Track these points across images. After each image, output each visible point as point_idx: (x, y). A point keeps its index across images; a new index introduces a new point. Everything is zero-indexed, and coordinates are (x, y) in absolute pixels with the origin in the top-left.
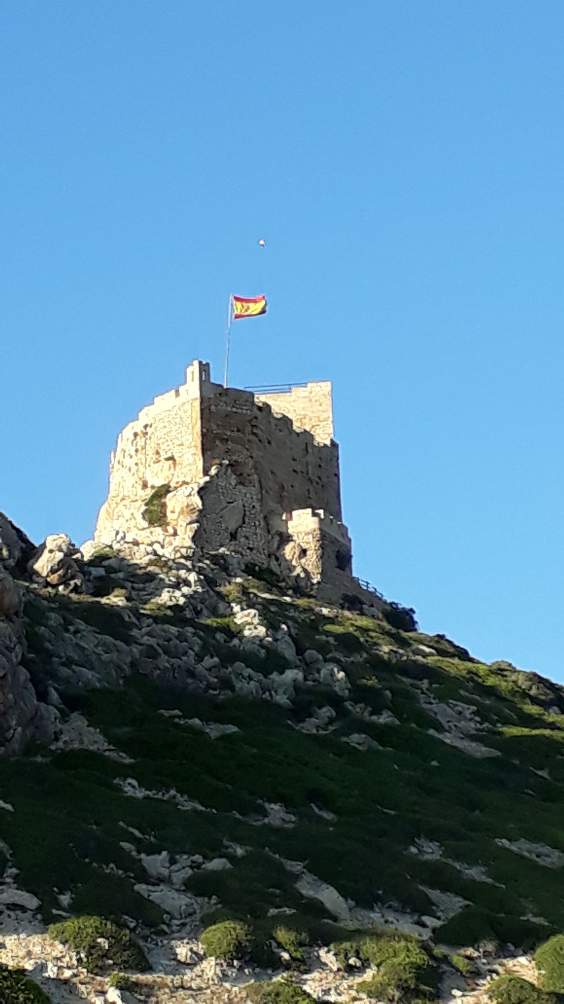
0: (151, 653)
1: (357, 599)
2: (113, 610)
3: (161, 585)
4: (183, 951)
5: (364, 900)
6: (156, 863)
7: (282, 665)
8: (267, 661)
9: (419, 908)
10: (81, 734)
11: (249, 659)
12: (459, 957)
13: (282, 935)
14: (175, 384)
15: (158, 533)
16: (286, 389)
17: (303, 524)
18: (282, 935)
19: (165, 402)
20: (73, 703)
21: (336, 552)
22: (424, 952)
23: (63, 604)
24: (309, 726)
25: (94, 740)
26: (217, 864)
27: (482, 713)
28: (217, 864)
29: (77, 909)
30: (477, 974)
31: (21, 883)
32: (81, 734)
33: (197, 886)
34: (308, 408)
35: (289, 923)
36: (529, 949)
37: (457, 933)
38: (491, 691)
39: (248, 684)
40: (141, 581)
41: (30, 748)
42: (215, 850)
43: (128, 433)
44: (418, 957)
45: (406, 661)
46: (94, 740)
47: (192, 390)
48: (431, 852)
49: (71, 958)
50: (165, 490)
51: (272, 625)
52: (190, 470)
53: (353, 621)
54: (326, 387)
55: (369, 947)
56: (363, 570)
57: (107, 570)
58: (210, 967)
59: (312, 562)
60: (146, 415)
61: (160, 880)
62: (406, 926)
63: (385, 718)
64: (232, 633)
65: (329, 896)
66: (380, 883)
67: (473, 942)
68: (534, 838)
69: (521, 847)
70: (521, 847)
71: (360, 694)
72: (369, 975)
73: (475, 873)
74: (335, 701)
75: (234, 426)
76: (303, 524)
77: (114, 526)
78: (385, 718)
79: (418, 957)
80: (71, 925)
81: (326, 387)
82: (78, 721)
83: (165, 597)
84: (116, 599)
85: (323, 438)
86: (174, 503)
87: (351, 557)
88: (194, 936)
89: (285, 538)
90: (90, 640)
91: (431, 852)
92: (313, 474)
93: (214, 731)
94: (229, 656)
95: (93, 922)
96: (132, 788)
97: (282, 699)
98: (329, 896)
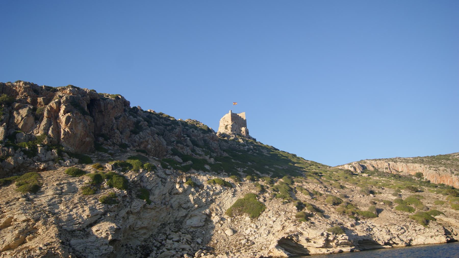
0: (231, 145)
1: (250, 138)
2: (225, 140)
3: (230, 137)
4: (245, 179)
5: (262, 173)
6: (239, 169)
7: (245, 146)
8: (244, 145)
9: (268, 174)
10: (225, 154)
11: (242, 145)
12: (275, 179)
13: (255, 177)
14: (228, 113)
15: (227, 130)
16: (240, 113)
17: (243, 129)
18: (255, 177)
19: (227, 115)
20: (224, 151)
21: (247, 132)
22: (76, 160)
23: (220, 139)
24: (249, 153)
25: (227, 155)
26: (245, 169)
27: (268, 151)
28: (245, 169)
29: (232, 175)
30: (277, 181)
31: (225, 172)
32: (225, 154)
33: (244, 172)
34: (242, 115)
35: (256, 176)
36: (282, 178)
37: (273, 177)
38: (267, 148)
39: (242, 148)
40: (229, 136)
41: (220, 156)
42: (245, 168)
43: (222, 118)
44: (270, 179)
45: (14, 90)
46: (227, 155)
47: (230, 113)
48: (267, 167)
49: (233, 180)
50: (227, 125)
51: (244, 141)
52: (230, 123)
53: (251, 140)
54: (244, 113)
55: (265, 178)
56: (250, 134)
57: (224, 135)
58: (248, 181)
59: (244, 133)
60: (224, 117)
61: (239, 171)
62: (267, 176)
63: (257, 152)
64: (239, 142)
65: (258, 173)
66: (265, 172)
67: (275, 177)
68: (278, 165)
69: (276, 166)
70: (276, 166)
71: (254, 149)
72: (265, 181)
73: (273, 169)
74: (252, 150)
75: (235, 117)
76: (243, 129)
77: (221, 130)
78: (257, 152)
79: (270, 179)
80: (232, 176)
81: (244, 113)
82: (225, 153)
83: (231, 138)
84: (226, 138)
85: (244, 119)
86: (228, 127)
87: (93, 93)
88: (245, 177)
89: (241, 131)
90: (224, 143)
91: (267, 167)
92: (244, 123)
93: (240, 154)
94: (240, 145)
95: (234, 176)
96: (233, 161)
97: (246, 150)
98: (258, 173)
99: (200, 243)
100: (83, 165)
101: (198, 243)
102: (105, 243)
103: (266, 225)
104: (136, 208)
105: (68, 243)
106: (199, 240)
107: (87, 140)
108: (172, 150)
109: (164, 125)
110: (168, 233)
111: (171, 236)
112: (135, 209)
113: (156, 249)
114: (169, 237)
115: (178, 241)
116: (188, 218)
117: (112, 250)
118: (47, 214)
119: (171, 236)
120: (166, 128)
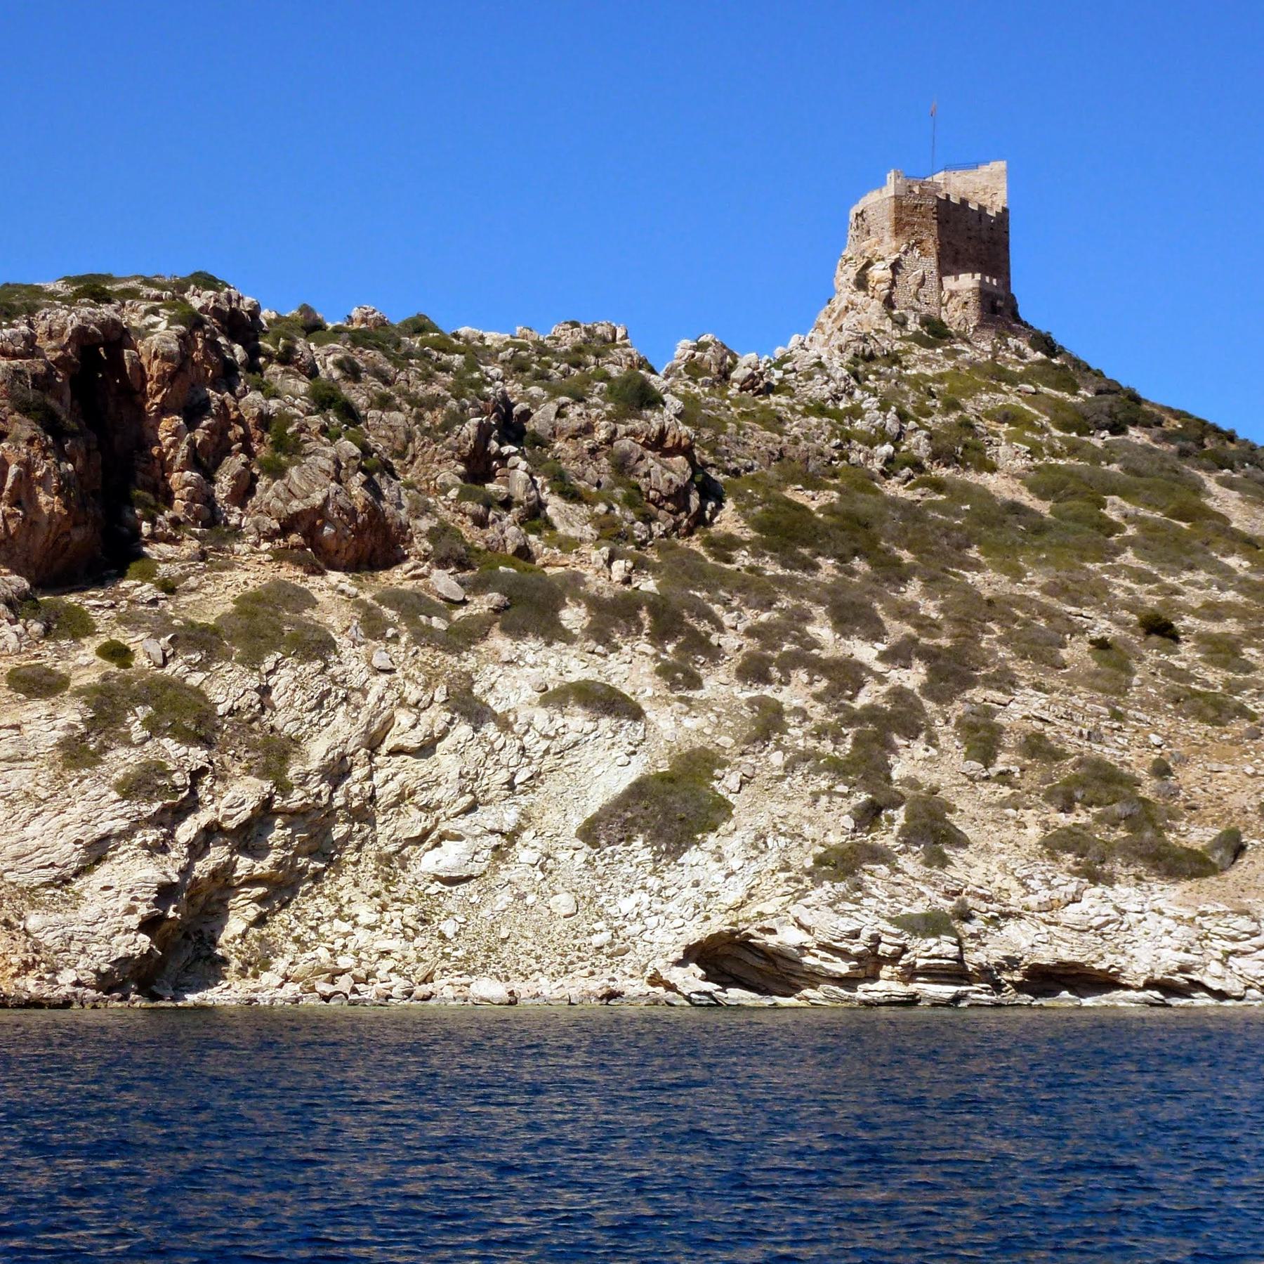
34: (984, 185)
54: (1000, 166)
99: (449, 935)
100: (64, 643)
101: (442, 937)
102: (125, 925)
103: (1154, 674)
104: (233, 811)
105: (21, 923)
106: (449, 928)
107: (76, 538)
108: (432, 535)
109: (414, 401)
110: (344, 896)
111: (354, 909)
112: (231, 817)
113: (294, 947)
114: (346, 910)
115: (371, 928)
116: (427, 844)
117: (146, 947)
118: (463, 408)
119: (354, 909)
120: (419, 418)
